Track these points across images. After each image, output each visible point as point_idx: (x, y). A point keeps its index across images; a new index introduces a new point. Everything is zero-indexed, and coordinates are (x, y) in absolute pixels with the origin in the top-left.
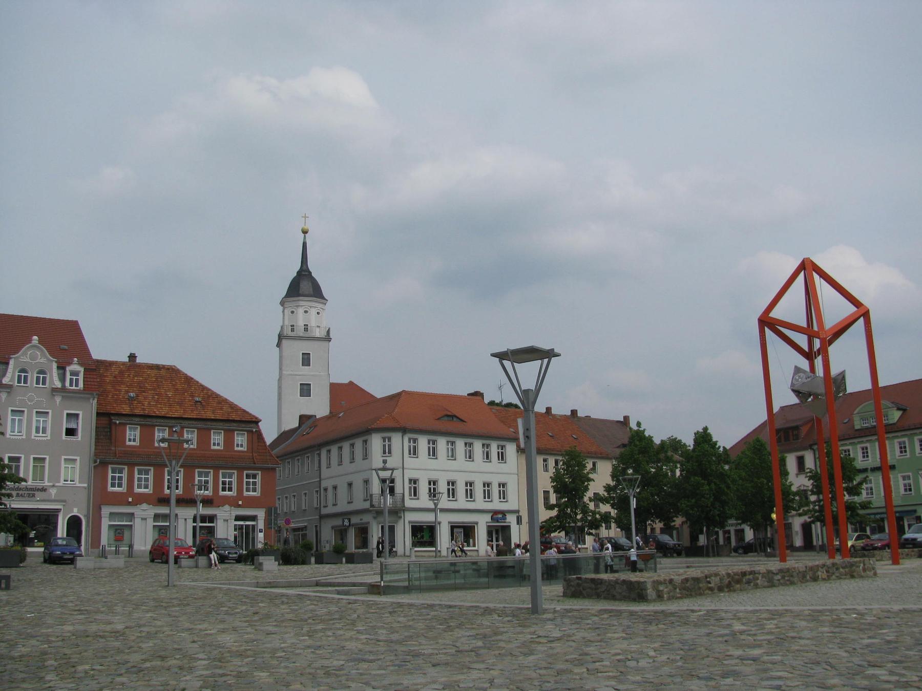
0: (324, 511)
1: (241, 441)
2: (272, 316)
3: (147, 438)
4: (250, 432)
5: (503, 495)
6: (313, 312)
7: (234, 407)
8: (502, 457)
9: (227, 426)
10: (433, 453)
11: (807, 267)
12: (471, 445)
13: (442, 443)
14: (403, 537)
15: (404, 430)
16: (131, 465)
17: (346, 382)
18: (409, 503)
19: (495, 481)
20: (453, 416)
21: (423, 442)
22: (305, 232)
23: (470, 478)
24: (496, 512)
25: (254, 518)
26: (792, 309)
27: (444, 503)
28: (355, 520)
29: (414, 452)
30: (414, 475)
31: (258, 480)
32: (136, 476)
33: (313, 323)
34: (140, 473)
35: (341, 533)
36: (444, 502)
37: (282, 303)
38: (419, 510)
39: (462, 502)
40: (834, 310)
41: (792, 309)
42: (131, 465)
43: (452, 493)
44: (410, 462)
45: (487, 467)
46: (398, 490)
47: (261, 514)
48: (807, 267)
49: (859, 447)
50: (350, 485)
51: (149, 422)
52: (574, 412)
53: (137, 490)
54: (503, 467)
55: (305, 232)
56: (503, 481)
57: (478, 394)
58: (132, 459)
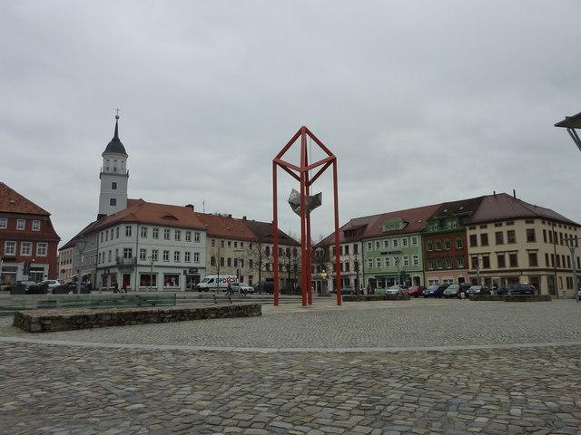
0: (99, 266)
1: (36, 226)
2: (98, 163)
3: (29, 225)
4: (43, 222)
5: (197, 259)
6: (119, 161)
7: (35, 207)
8: (197, 239)
9: (27, 217)
10: (178, 238)
11: (304, 131)
12: (168, 231)
13: (162, 231)
14: (135, 280)
15: (139, 223)
16: (35, 243)
17: (183, 204)
18: (140, 262)
19: (192, 252)
20: (172, 216)
21: (150, 230)
22: (117, 118)
23: (166, 249)
24: (191, 268)
25: (42, 269)
26: (293, 157)
27: (161, 261)
28: (111, 271)
29: (144, 235)
30: (143, 247)
31: (46, 247)
32: (22, 247)
33: (119, 167)
34: (40, 245)
35: (105, 277)
36: (161, 261)
37: (103, 155)
38: (144, 266)
39: (172, 262)
40: (316, 155)
41: (293, 157)
42: (35, 243)
43: (166, 257)
44: (142, 240)
45: (188, 244)
46: (134, 255)
47: (46, 267)
48: (304, 131)
49: (402, 239)
50: (110, 252)
51: (14, 216)
52: (245, 218)
53: (37, 255)
54: (197, 244)
55: (117, 118)
56: (197, 251)
57: (191, 207)
58: (535, 281)
